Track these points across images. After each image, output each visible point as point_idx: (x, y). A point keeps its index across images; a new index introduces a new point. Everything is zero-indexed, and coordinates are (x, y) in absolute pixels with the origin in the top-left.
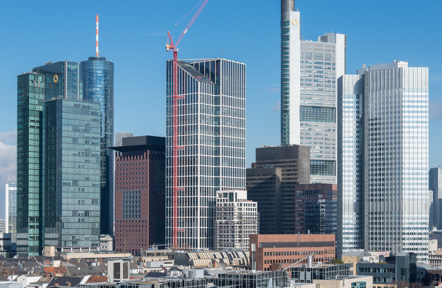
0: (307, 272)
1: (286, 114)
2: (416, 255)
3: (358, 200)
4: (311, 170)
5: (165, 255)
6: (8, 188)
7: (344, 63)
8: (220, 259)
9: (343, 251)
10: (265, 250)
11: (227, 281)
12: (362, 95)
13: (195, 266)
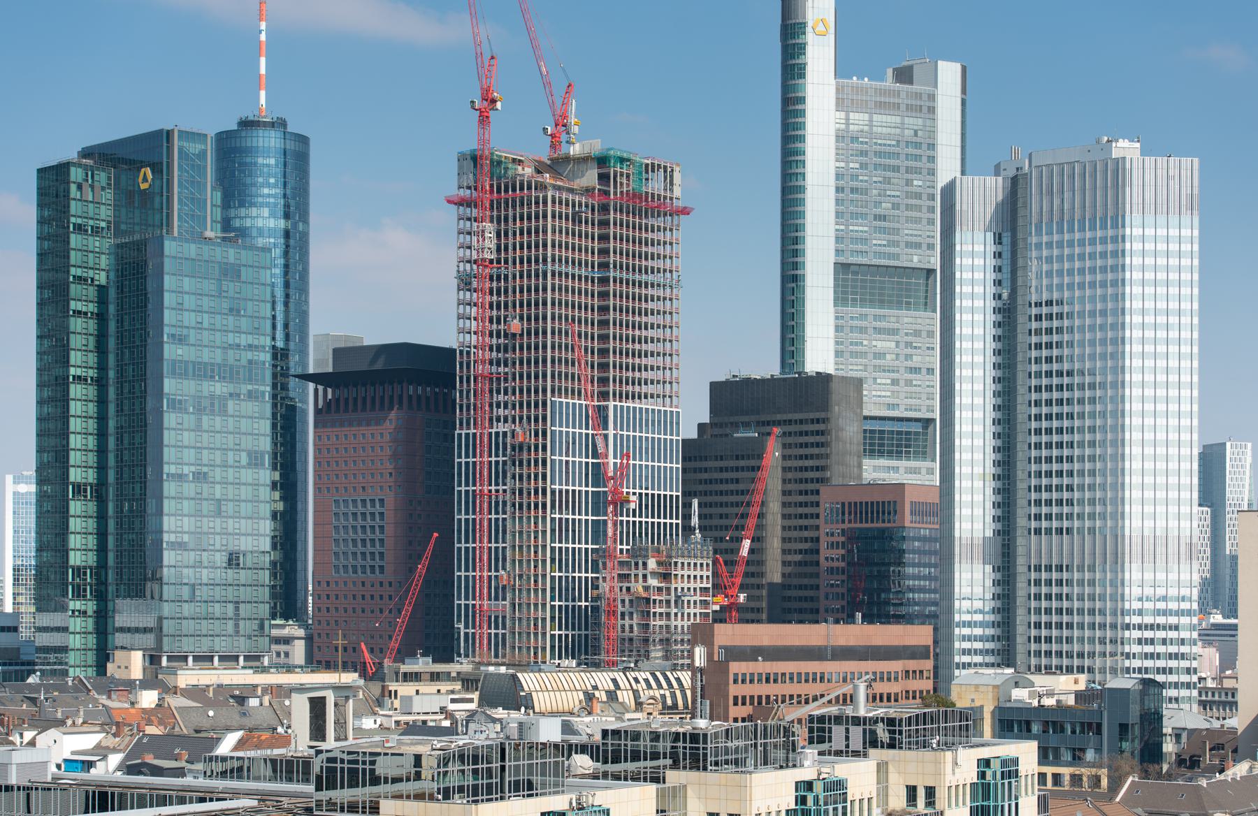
0: (852, 728)
1: (794, 285)
2: (1162, 686)
3: (999, 531)
4: (865, 444)
5: (454, 679)
6: (10, 487)
7: (959, 143)
8: (609, 693)
9: (957, 672)
10: (736, 667)
11: (626, 751)
12: (1009, 234)
13: (537, 710)
